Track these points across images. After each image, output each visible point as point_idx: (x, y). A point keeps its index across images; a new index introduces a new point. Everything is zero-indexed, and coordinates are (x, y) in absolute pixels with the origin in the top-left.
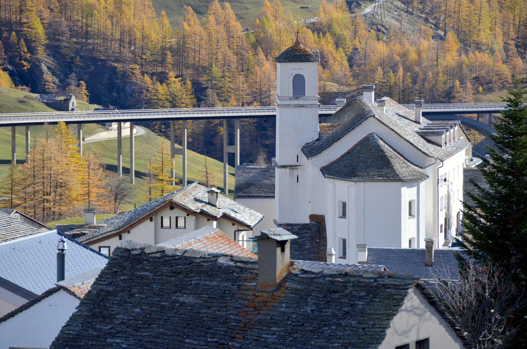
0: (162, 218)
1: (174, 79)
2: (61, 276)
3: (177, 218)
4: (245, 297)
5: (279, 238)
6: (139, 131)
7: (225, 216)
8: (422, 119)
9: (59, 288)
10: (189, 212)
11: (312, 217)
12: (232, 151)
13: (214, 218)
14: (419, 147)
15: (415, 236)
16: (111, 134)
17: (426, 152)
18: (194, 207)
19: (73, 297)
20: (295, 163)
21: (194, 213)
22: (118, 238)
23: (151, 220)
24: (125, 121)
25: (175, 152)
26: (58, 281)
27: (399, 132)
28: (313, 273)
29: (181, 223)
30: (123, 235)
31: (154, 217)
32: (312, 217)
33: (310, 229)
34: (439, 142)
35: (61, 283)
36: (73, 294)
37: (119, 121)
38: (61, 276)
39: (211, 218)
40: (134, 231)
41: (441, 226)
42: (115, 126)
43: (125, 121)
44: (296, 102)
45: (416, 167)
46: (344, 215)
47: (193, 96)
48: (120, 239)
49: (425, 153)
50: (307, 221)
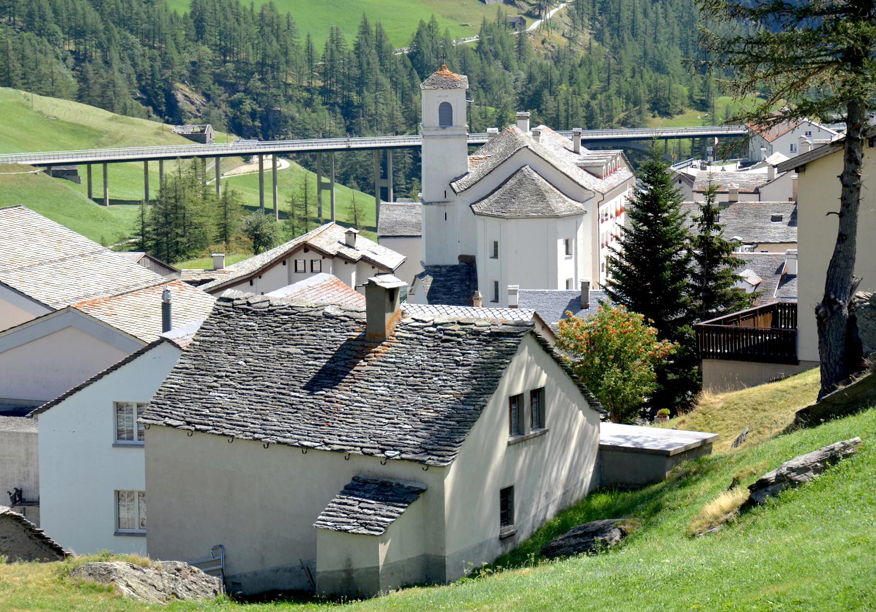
0: (296, 261)
1: (321, 107)
2: (166, 327)
3: (312, 261)
4: (353, 348)
5: (388, 286)
6: (284, 164)
7: (364, 259)
8: (582, 149)
9: (162, 340)
10: (325, 255)
11: (461, 258)
12: (385, 186)
13: (353, 261)
14: (577, 180)
15: (573, 276)
16: (253, 167)
17: (585, 185)
18: (332, 249)
19: (177, 349)
20: (443, 199)
21: (331, 256)
22: (249, 283)
23: (284, 264)
24: (268, 153)
25: (322, 186)
26: (164, 331)
27: (554, 163)
28: (423, 322)
29: (316, 266)
30: (254, 281)
31: (287, 261)
32: (461, 258)
33: (459, 271)
34: (599, 174)
35: (166, 335)
36: (178, 346)
37: (260, 154)
38: (166, 327)
39: (348, 260)
40: (837, 188)
41: (603, 264)
42: (256, 159)
43: (268, 153)
44: (443, 132)
45: (573, 202)
46: (496, 256)
47: (342, 125)
48: (251, 284)
49: (582, 187)
50: (457, 263)
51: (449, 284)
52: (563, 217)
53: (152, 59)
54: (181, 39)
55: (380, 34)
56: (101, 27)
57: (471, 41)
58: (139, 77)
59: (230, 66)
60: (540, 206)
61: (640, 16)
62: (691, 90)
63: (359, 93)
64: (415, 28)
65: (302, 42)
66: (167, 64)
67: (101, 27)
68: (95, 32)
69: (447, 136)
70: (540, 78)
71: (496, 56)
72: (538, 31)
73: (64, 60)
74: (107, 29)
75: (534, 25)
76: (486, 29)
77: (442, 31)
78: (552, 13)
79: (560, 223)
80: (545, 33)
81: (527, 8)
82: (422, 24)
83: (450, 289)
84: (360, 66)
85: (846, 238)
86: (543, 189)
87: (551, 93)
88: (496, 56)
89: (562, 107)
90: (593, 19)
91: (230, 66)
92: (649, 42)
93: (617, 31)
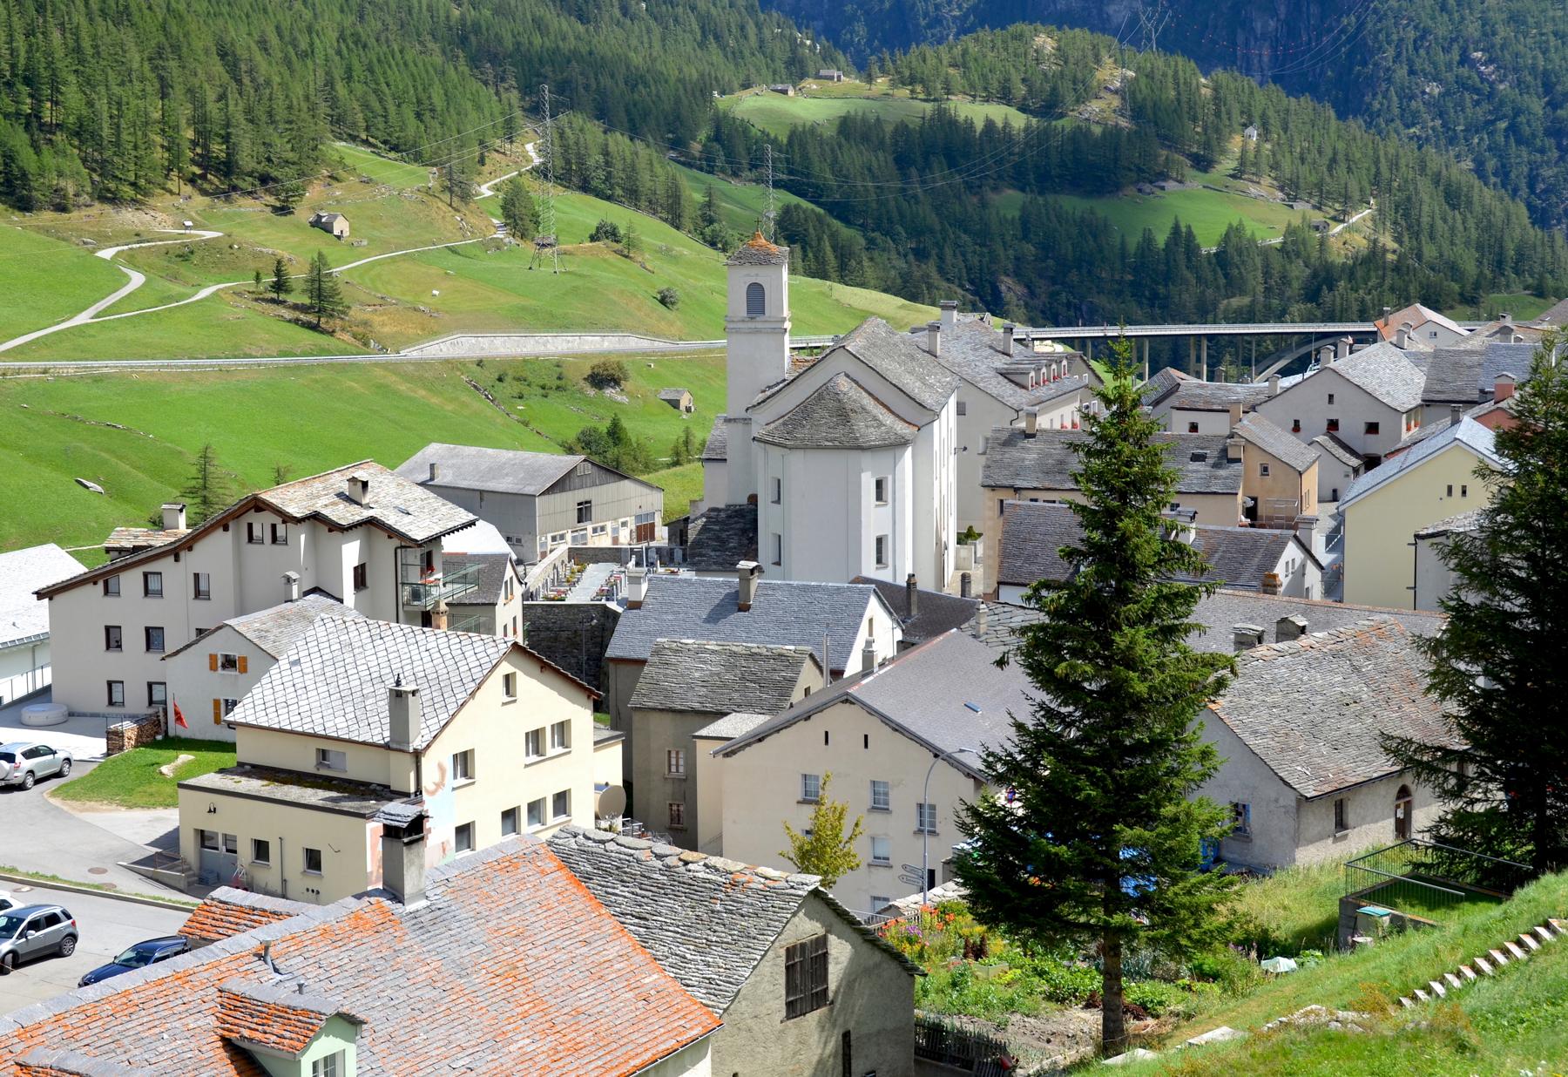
22: (172, 558)
30: (183, 554)
31: (231, 525)
44: (752, 325)
46: (778, 501)
51: (724, 535)
52: (870, 448)
53: (982, 255)
54: (1008, 238)
55: (1190, 234)
56: (938, 227)
57: (1277, 241)
58: (969, 269)
59: (1051, 262)
60: (839, 432)
61: (1439, 222)
62: (1462, 287)
63: (1166, 285)
64: (1223, 230)
65: (1118, 241)
66: (994, 259)
67: (938, 227)
68: (932, 231)
69: (757, 331)
70: (1323, 274)
71: (1298, 255)
72: (1340, 234)
73: (905, 256)
74: (943, 230)
75: (1338, 228)
76: (1290, 232)
77: (1248, 233)
78: (1355, 219)
79: (866, 458)
80: (1347, 236)
81: (1333, 213)
82: (1230, 226)
83: (723, 542)
84: (1168, 262)
85: (84, 715)
86: (848, 407)
87: (1330, 289)
88: (1298, 255)
89: (1338, 301)
90: (1395, 223)
91: (1051, 262)
92: (1446, 245)
93: (1416, 235)
